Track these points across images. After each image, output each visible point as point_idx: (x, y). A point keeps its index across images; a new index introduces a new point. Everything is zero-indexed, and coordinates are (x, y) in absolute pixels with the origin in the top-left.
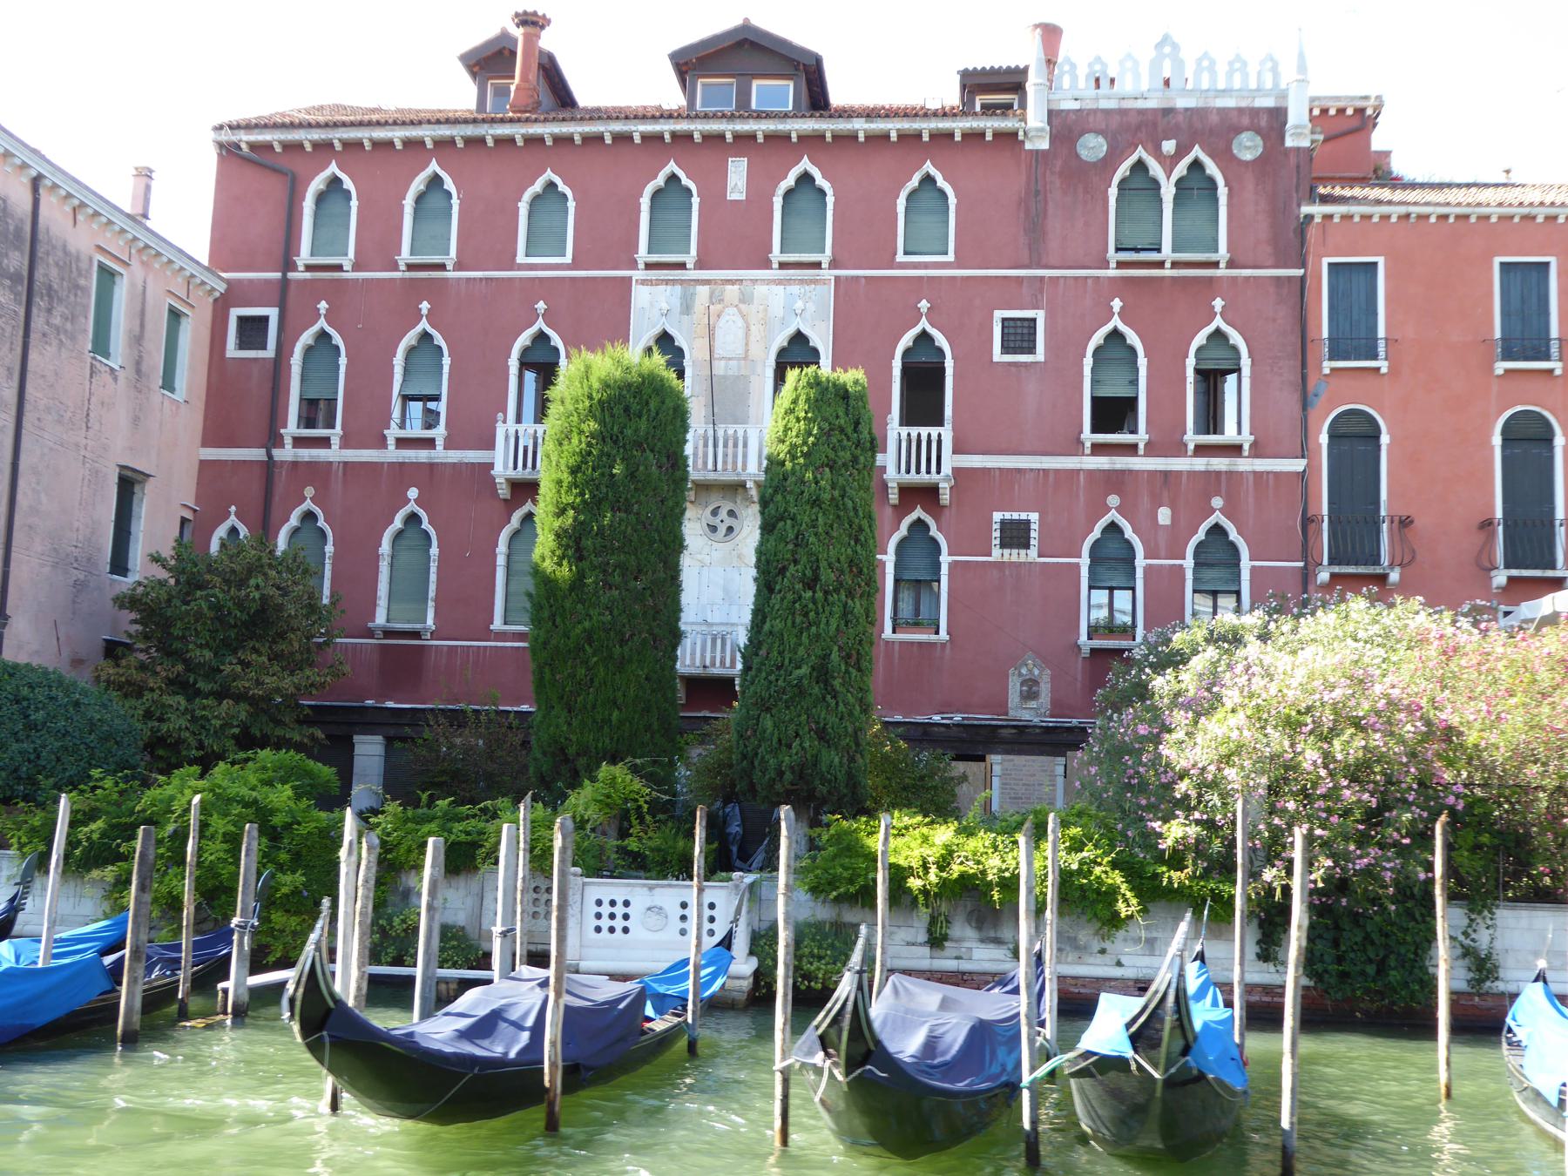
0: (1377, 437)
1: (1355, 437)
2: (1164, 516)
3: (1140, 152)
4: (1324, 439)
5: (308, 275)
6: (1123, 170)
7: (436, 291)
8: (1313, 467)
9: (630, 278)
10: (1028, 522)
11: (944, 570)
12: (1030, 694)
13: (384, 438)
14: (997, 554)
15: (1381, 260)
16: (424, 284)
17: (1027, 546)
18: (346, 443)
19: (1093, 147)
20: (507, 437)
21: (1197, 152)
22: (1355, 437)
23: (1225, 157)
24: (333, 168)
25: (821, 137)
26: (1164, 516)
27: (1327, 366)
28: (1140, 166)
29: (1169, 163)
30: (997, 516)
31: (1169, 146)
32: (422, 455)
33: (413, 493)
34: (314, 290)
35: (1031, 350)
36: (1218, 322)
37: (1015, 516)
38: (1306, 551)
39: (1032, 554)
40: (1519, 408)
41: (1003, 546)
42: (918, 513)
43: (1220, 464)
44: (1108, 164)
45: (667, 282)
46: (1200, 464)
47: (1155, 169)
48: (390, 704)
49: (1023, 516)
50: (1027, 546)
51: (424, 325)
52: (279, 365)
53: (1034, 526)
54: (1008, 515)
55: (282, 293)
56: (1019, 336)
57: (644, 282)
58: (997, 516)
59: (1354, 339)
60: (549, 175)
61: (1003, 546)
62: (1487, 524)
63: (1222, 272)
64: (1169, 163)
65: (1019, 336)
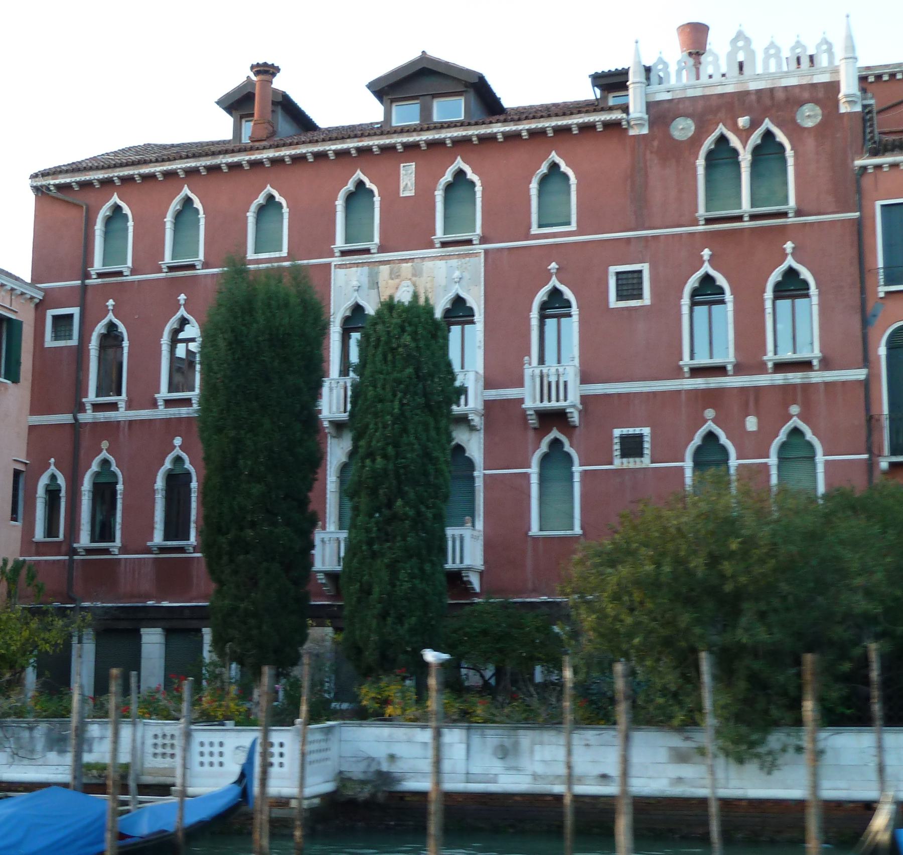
2: (751, 423)
4: (882, 351)
9: (329, 264)
11: (577, 478)
14: (619, 463)
17: (641, 455)
18: (130, 406)
19: (683, 128)
21: (767, 124)
23: (794, 130)
24: (115, 199)
26: (751, 423)
27: (882, 290)
30: (617, 432)
33: (178, 441)
34: (105, 291)
35: (640, 296)
38: (872, 449)
39: (646, 462)
42: (555, 434)
43: (795, 378)
44: (695, 141)
45: (357, 265)
46: (779, 379)
47: (735, 141)
49: (637, 431)
50: (641, 455)
52: (81, 351)
53: (647, 439)
55: (82, 296)
56: (629, 286)
57: (340, 266)
60: (269, 189)
63: (791, 220)
64: (744, 136)
65: (629, 286)
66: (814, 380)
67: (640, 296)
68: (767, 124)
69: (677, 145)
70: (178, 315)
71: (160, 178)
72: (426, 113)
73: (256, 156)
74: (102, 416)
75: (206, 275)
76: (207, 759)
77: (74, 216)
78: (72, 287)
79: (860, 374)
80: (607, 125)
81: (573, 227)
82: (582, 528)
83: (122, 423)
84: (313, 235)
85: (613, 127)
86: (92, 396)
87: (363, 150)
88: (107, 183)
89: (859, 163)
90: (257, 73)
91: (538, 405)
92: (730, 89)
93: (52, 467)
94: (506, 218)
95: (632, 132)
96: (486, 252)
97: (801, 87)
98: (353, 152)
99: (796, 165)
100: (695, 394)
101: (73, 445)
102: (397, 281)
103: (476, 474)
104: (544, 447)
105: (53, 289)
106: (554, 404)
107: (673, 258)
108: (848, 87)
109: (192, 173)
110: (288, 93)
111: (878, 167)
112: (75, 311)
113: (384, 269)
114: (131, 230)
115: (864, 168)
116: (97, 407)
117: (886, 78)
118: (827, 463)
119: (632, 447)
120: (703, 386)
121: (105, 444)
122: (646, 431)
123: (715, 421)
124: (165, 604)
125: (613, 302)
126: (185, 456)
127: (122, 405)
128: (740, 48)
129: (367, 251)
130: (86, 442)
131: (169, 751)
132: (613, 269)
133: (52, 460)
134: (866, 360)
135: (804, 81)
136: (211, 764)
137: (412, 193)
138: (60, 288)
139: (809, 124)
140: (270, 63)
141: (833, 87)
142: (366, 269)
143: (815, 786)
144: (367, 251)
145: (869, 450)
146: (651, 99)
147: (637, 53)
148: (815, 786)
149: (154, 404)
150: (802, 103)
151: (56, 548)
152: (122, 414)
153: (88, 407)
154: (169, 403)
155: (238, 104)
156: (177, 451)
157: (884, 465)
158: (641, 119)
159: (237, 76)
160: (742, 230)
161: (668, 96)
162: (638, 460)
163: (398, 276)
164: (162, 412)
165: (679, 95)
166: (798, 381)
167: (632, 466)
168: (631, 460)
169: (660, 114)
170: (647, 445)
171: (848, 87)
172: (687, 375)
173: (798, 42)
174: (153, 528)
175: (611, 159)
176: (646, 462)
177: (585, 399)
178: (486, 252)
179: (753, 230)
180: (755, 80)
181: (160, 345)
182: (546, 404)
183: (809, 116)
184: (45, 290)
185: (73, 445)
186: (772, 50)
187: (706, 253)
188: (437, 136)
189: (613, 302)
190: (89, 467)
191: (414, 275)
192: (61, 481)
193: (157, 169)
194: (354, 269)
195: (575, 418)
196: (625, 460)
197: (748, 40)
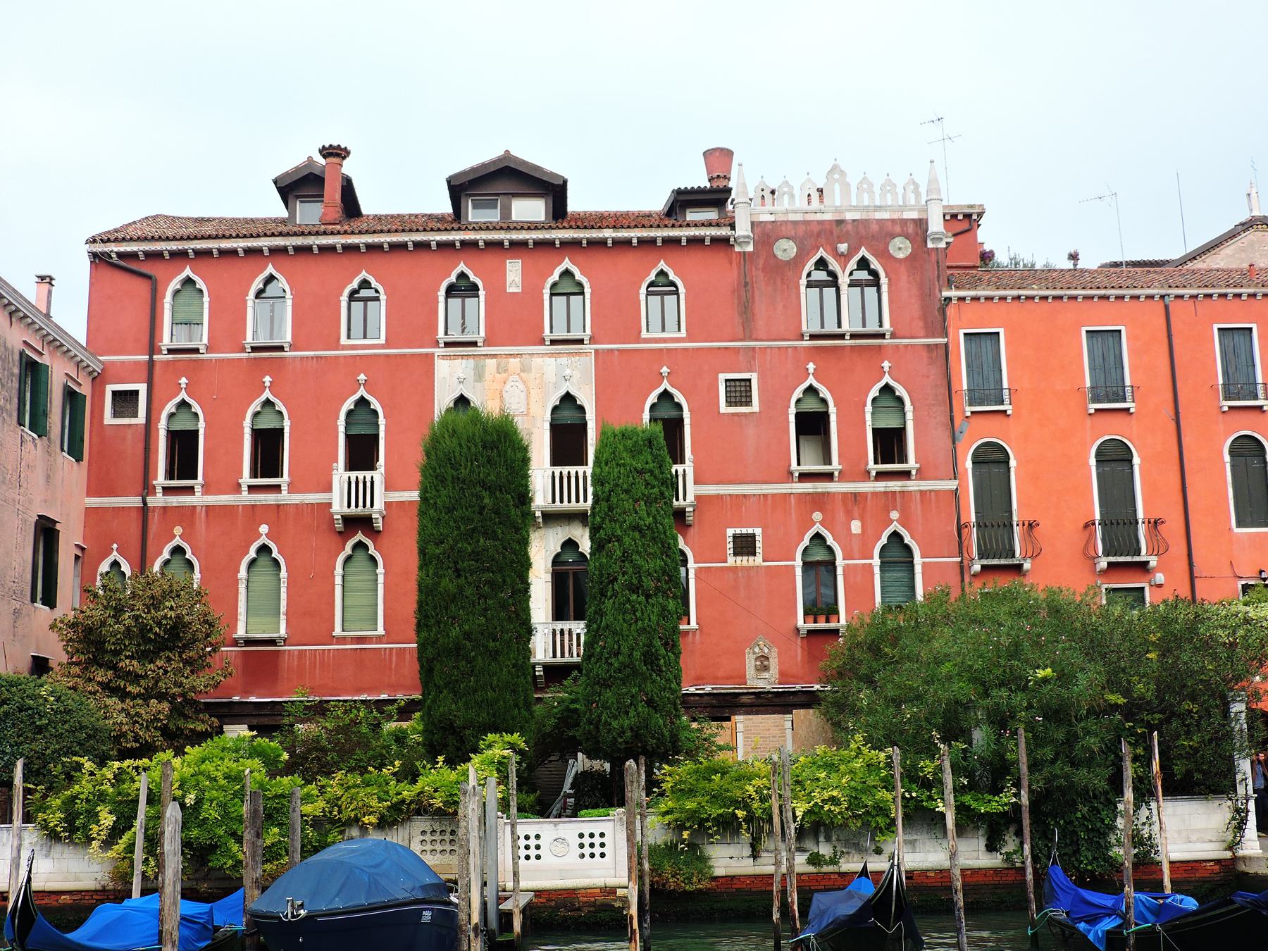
2: (856, 527)
4: (969, 464)
5: (170, 357)
9: (433, 354)
13: (239, 485)
18: (292, 488)
19: (786, 249)
22: (992, 460)
23: (884, 255)
24: (188, 272)
26: (856, 527)
27: (969, 409)
29: (843, 258)
33: (264, 529)
35: (748, 403)
37: (744, 531)
41: (735, 554)
42: (360, 537)
43: (895, 485)
44: (799, 261)
46: (881, 486)
47: (834, 265)
49: (750, 531)
54: (738, 531)
58: (730, 532)
59: (987, 390)
61: (735, 554)
64: (843, 258)
66: (911, 489)
67: (748, 403)
68: (864, 252)
70: (263, 398)
72: (506, 212)
73: (653, 233)
74: (174, 500)
75: (294, 358)
76: (587, 840)
77: (141, 288)
78: (136, 363)
79: (952, 485)
80: (715, 240)
81: (382, 340)
83: (198, 510)
84: (413, 325)
85: (723, 242)
86: (160, 479)
87: (405, 244)
88: (180, 255)
89: (946, 294)
90: (325, 157)
91: (346, 510)
93: (115, 553)
94: (617, 319)
95: (737, 249)
97: (893, 221)
98: (458, 244)
99: (890, 292)
100: (802, 497)
102: (504, 375)
104: (348, 549)
105: (113, 362)
108: (936, 225)
109: (275, 251)
111: (962, 299)
112: (142, 388)
113: (491, 363)
114: (206, 305)
115: (949, 299)
116: (167, 490)
117: (960, 217)
118: (924, 564)
119: (745, 545)
120: (811, 491)
121: (178, 530)
123: (822, 523)
124: (253, 699)
125: (723, 408)
128: (836, 181)
129: (474, 344)
130: (154, 527)
132: (722, 377)
133: (115, 546)
135: (895, 216)
136: (582, 846)
137: (519, 290)
138: (123, 362)
139: (901, 255)
140: (335, 144)
141: (921, 224)
142: (471, 361)
144: (474, 344)
145: (961, 554)
146: (755, 219)
149: (237, 488)
150: (893, 236)
152: (198, 499)
153: (159, 490)
155: (297, 186)
156: (263, 540)
157: (977, 567)
158: (748, 237)
159: (298, 152)
160: (843, 347)
161: (772, 218)
162: (751, 558)
163: (506, 371)
164: (246, 498)
166: (898, 489)
167: (745, 563)
168: (745, 558)
169: (766, 234)
171: (936, 225)
172: (796, 480)
173: (865, 179)
174: (236, 620)
175: (718, 274)
176: (758, 560)
177: (388, 505)
178: (596, 351)
179: (168, 362)
180: (850, 211)
181: (243, 428)
186: (888, 186)
187: (811, 367)
188: (547, 236)
189: (723, 408)
190: (161, 553)
191: (523, 370)
193: (240, 244)
194: (459, 361)
195: (379, 525)
196: (739, 558)
197: (842, 173)
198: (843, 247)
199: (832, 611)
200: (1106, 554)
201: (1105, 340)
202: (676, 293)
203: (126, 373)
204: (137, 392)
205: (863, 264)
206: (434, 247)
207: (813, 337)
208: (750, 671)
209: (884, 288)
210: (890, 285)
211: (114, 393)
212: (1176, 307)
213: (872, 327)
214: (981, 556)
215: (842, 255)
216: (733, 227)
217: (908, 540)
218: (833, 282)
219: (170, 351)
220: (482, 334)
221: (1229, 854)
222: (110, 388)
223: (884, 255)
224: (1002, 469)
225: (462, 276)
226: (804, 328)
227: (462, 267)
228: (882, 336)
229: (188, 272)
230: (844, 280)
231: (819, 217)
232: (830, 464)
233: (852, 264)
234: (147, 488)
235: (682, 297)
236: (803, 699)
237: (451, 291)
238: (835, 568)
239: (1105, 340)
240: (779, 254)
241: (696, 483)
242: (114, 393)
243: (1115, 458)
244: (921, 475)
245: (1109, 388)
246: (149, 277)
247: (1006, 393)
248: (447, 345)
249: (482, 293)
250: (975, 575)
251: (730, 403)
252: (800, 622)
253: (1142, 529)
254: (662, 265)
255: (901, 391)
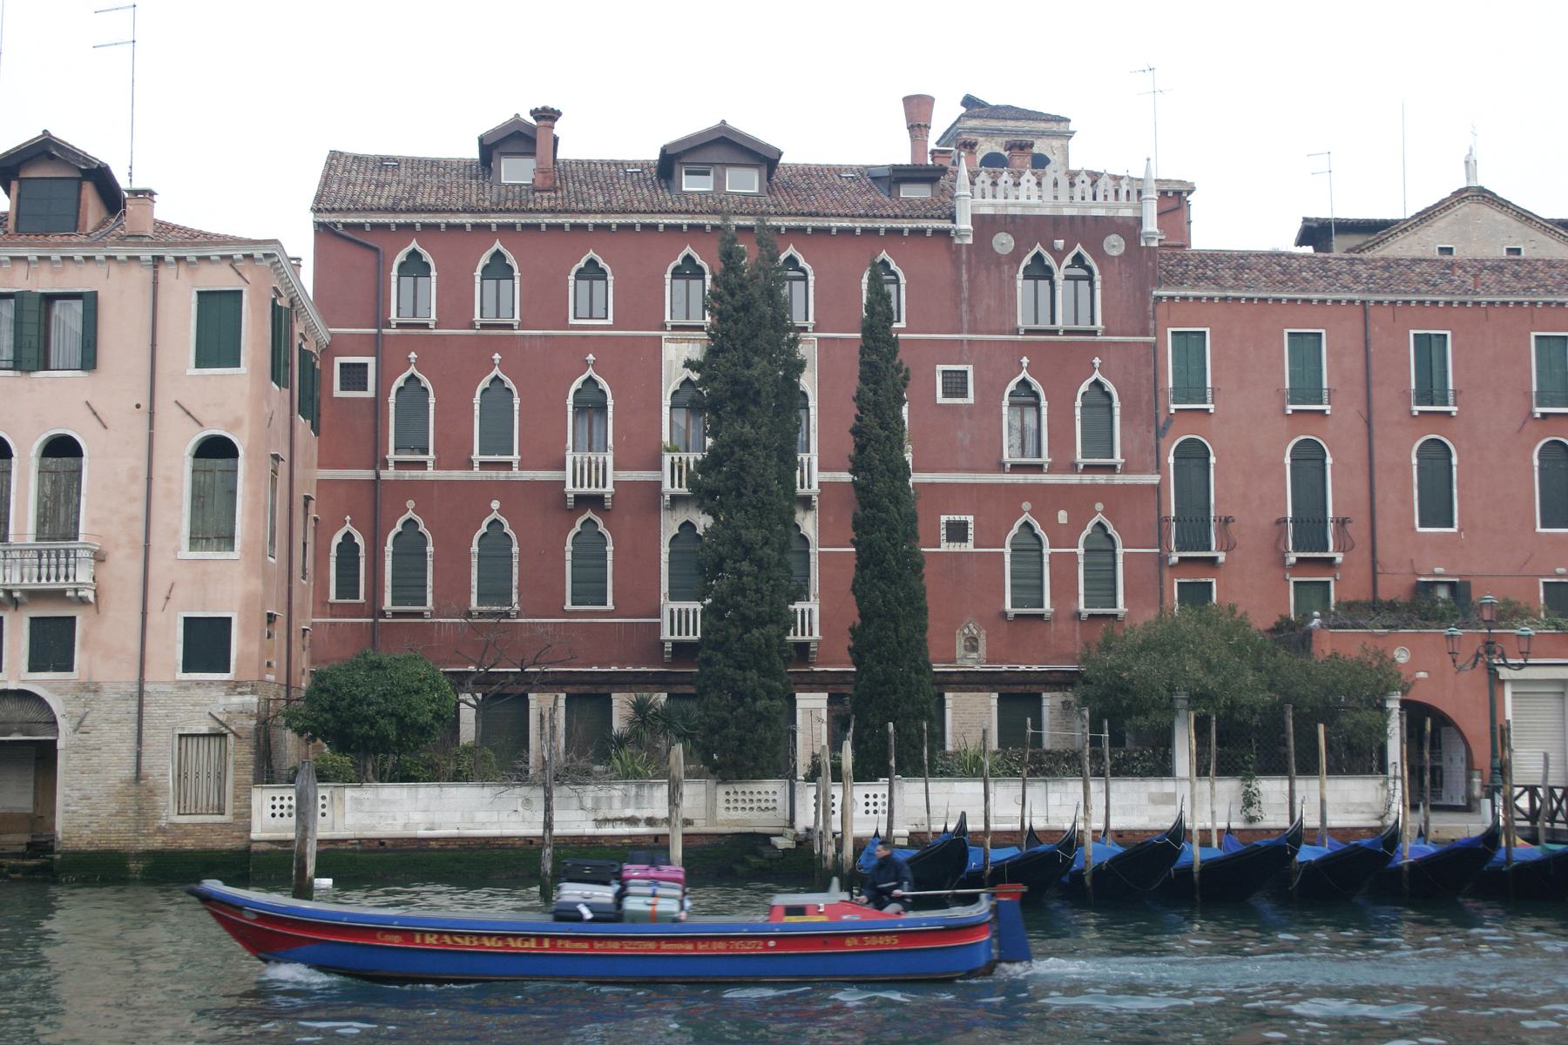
0: (1324, 460)
1: (1193, 455)
2: (1063, 517)
3: (1038, 248)
4: (1171, 460)
5: (398, 331)
6: (1027, 260)
7: (508, 345)
8: (1165, 480)
9: (660, 338)
10: (966, 523)
11: (1046, 560)
12: (972, 645)
13: (472, 462)
14: (945, 547)
15: (1208, 330)
16: (496, 337)
17: (965, 540)
18: (437, 466)
19: (1004, 242)
20: (672, 465)
21: (1079, 248)
22: (1193, 455)
23: (1099, 255)
24: (414, 245)
25: (804, 230)
26: (1063, 517)
27: (1173, 407)
28: (1038, 258)
29: (1059, 256)
30: (944, 518)
31: (1060, 244)
32: (502, 475)
33: (495, 505)
34: (407, 343)
35: (964, 395)
36: (1097, 375)
37: (957, 518)
38: (1161, 540)
39: (969, 547)
40: (1296, 440)
41: (948, 540)
42: (589, 514)
43: (1101, 479)
44: (1016, 257)
45: (689, 340)
46: (1087, 479)
47: (1049, 260)
48: (629, 669)
49: (963, 518)
50: (965, 540)
51: (496, 371)
52: (378, 404)
53: (971, 526)
54: (951, 518)
55: (376, 345)
56: (955, 385)
57: (670, 340)
58: (944, 518)
59: (1190, 387)
60: (591, 254)
61: (948, 540)
62: (1282, 521)
63: (1099, 338)
64: (1059, 256)
65: (955, 385)
67: (964, 395)
68: (1079, 248)
69: (997, 260)
70: (493, 375)
71: (368, 229)
73: (897, 224)
75: (523, 336)
76: (732, 805)
77: (364, 259)
80: (936, 232)
81: (610, 321)
82: (614, 603)
85: (944, 234)
92: (1047, 212)
96: (819, 339)
101: (374, 503)
103: (811, 550)
106: (593, 490)
107: (995, 363)
110: (897, 162)
111: (1171, 298)
122: (970, 519)
126: (503, 520)
127: (430, 464)
131: (771, 805)
134: (1159, 467)
139: (1115, 253)
143: (548, 825)
147: (1148, 169)
148: (548, 825)
149: (469, 465)
151: (357, 611)
154: (484, 465)
164: (477, 474)
165: (1028, 212)
167: (957, 549)
170: (971, 532)
178: (819, 339)
179: (397, 336)
182: (585, 490)
183: (1115, 245)
184: (332, 335)
185: (374, 503)
192: (359, 539)
193: (467, 219)
198: (1060, 244)
199: (506, 597)
200: (1296, 549)
201: (1305, 347)
202: (805, 279)
203: (356, 344)
204: (365, 365)
205: (1078, 259)
206: (543, 228)
207: (1028, 332)
208: (960, 651)
209: (1098, 285)
210: (1103, 282)
211: (342, 365)
212: (1374, 313)
213: (1084, 325)
214: (1296, 549)
215: (1058, 251)
216: (954, 222)
217: (1111, 530)
218: (1048, 274)
219: (399, 326)
220: (433, 316)
221: (1378, 823)
222: (338, 360)
223: (1099, 255)
224: (1318, 463)
225: (688, 258)
226: (1020, 323)
227: (688, 250)
228: (1094, 333)
229: (414, 245)
230: (1059, 275)
231: (1037, 212)
232: (1112, 457)
233: (1068, 260)
234: (379, 462)
235: (811, 284)
236: (960, 678)
237: (677, 273)
238: (1041, 556)
239: (1305, 347)
240: (997, 248)
241: (821, 469)
242: (342, 365)
243: (1309, 458)
244: (1126, 470)
245: (1307, 387)
246: (376, 250)
247: (1450, 393)
248: (674, 328)
249: (433, 273)
250: (1172, 566)
251: (946, 394)
252: (1082, 607)
253: (1331, 527)
254: (688, 250)
255: (1037, 386)
